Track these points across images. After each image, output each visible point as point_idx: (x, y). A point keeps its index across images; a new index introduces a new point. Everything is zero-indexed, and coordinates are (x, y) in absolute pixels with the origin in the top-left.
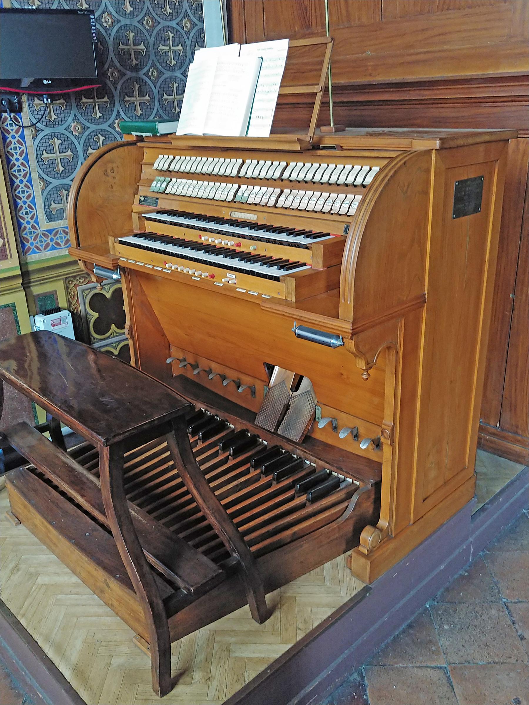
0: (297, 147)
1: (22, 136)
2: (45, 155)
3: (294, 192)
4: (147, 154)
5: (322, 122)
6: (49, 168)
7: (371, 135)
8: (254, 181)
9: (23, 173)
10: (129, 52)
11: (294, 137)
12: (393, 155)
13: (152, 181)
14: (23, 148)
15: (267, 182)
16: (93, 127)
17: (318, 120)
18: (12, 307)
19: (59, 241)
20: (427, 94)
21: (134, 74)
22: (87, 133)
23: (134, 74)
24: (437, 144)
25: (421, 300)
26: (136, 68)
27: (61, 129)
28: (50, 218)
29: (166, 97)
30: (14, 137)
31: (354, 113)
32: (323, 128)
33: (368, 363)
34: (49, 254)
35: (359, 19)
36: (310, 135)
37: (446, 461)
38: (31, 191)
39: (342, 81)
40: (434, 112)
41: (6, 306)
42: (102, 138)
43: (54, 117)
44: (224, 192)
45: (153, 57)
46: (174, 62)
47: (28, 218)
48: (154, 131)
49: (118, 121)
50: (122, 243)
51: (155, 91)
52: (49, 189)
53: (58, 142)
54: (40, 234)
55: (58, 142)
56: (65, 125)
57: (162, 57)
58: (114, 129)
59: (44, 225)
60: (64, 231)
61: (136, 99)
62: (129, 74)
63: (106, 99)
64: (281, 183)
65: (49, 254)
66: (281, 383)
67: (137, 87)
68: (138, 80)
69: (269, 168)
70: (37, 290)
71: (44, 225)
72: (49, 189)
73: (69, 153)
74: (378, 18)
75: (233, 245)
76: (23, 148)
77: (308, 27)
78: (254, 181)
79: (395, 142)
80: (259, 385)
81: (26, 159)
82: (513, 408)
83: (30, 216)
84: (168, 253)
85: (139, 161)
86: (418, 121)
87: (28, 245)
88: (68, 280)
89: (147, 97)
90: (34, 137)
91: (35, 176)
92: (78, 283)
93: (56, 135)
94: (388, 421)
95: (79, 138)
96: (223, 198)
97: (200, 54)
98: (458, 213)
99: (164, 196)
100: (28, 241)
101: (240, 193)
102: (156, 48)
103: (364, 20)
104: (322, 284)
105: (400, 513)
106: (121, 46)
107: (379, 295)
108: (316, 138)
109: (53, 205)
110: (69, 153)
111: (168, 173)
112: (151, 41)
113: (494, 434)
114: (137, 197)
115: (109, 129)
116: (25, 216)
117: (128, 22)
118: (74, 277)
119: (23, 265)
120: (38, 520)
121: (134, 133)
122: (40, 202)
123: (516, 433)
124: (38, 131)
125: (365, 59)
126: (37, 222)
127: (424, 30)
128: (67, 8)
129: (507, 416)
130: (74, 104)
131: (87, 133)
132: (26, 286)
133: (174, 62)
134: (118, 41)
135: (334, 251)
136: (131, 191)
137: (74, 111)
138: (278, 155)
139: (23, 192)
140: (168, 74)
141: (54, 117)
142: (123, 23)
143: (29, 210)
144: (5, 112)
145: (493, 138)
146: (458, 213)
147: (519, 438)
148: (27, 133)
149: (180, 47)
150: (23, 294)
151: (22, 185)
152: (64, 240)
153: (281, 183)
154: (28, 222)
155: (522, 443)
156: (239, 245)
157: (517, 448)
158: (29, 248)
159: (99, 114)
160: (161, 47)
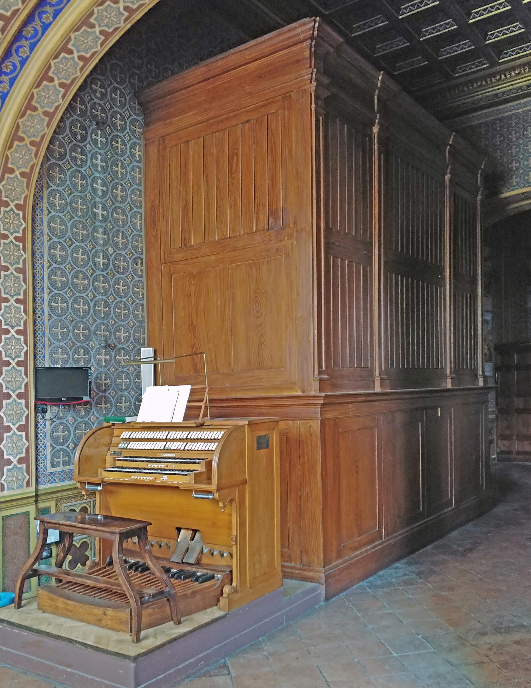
0: (195, 425)
1: (45, 425)
2: (55, 434)
3: (193, 443)
4: (116, 432)
5: (205, 415)
6: (55, 440)
7: (224, 420)
8: (174, 440)
9: (43, 443)
10: (102, 383)
11: (193, 421)
12: (230, 427)
13: (119, 444)
14: (45, 430)
15: (180, 440)
16: (80, 420)
17: (203, 415)
18: (27, 514)
19: (55, 479)
20: (254, 403)
21: (103, 394)
22: (77, 423)
23: (103, 394)
24: (247, 423)
25: (245, 482)
26: (105, 391)
27: (64, 421)
28: (53, 466)
29: (118, 404)
30: (41, 425)
31: (220, 411)
32: (205, 418)
33: (224, 504)
34: (50, 485)
35: (223, 371)
36: (200, 421)
37: (264, 562)
38: (45, 452)
39: (215, 397)
40: (258, 410)
41: (25, 513)
42: (84, 425)
43: (61, 415)
44: (159, 446)
45: (113, 385)
46: (124, 387)
47: (41, 465)
48: (124, 421)
49: (95, 417)
50: (105, 471)
51: (113, 401)
52: (54, 451)
53: (62, 427)
54: (47, 474)
55: (62, 427)
56: (66, 419)
57: (118, 386)
58: (91, 420)
59: (50, 469)
60: (59, 473)
61: (103, 406)
62: (101, 394)
63: (88, 406)
64: (187, 440)
65: (50, 485)
66: (185, 539)
67: (104, 400)
68: (105, 396)
69: (182, 435)
70: (41, 505)
71: (50, 469)
72: (54, 451)
73: (67, 432)
74: (231, 371)
75: (57, 600)
76: (45, 430)
77: (198, 373)
78: (174, 440)
79: (231, 423)
80: (172, 543)
81: (45, 436)
82: (307, 552)
83: (43, 465)
84: (133, 472)
85: (112, 435)
86: (252, 415)
87: (40, 480)
88: (58, 501)
89: (109, 405)
90: (51, 425)
91: (48, 444)
92: (62, 502)
93: (61, 424)
94: (234, 533)
95: (72, 425)
96: (158, 448)
97: (147, 388)
98: (259, 448)
99: (125, 450)
100: (40, 478)
101: (167, 446)
102: (115, 380)
103: (225, 371)
104: (205, 477)
105: (242, 581)
106: (98, 381)
107: (227, 481)
108: (202, 422)
109: (55, 459)
110: (67, 432)
111: (129, 440)
112: (113, 378)
113: (300, 569)
114: (109, 453)
115: (88, 421)
116: (40, 465)
117: (102, 370)
118: (61, 499)
119: (37, 491)
120: (60, 603)
121: (111, 422)
122: (49, 457)
123: (310, 566)
124: (53, 422)
125: (226, 388)
126: (46, 468)
127: (252, 377)
128: (75, 366)
129: (305, 558)
130: (72, 409)
131: (77, 423)
132: (36, 502)
133: (124, 387)
134: (97, 378)
135: (209, 464)
136: (106, 449)
137: (72, 412)
138: (186, 429)
139: (41, 452)
140: (120, 393)
141: (61, 415)
142: (100, 370)
143: (43, 461)
144: (40, 413)
145: (271, 420)
146: (259, 448)
147: (311, 568)
148: (48, 423)
149: (128, 380)
150: (34, 506)
151: (41, 449)
152: (58, 478)
153: (187, 440)
154: (42, 468)
155: (313, 571)
156: (167, 466)
157: (310, 574)
158: (40, 482)
159: (84, 413)
160: (118, 380)
